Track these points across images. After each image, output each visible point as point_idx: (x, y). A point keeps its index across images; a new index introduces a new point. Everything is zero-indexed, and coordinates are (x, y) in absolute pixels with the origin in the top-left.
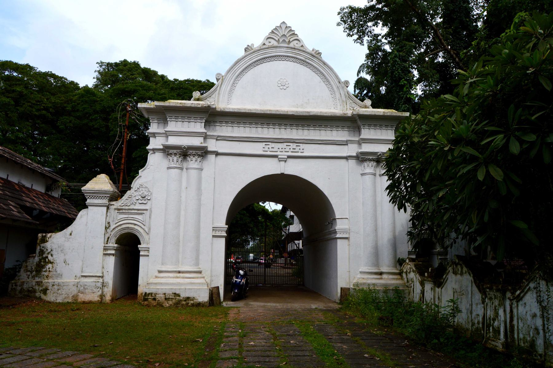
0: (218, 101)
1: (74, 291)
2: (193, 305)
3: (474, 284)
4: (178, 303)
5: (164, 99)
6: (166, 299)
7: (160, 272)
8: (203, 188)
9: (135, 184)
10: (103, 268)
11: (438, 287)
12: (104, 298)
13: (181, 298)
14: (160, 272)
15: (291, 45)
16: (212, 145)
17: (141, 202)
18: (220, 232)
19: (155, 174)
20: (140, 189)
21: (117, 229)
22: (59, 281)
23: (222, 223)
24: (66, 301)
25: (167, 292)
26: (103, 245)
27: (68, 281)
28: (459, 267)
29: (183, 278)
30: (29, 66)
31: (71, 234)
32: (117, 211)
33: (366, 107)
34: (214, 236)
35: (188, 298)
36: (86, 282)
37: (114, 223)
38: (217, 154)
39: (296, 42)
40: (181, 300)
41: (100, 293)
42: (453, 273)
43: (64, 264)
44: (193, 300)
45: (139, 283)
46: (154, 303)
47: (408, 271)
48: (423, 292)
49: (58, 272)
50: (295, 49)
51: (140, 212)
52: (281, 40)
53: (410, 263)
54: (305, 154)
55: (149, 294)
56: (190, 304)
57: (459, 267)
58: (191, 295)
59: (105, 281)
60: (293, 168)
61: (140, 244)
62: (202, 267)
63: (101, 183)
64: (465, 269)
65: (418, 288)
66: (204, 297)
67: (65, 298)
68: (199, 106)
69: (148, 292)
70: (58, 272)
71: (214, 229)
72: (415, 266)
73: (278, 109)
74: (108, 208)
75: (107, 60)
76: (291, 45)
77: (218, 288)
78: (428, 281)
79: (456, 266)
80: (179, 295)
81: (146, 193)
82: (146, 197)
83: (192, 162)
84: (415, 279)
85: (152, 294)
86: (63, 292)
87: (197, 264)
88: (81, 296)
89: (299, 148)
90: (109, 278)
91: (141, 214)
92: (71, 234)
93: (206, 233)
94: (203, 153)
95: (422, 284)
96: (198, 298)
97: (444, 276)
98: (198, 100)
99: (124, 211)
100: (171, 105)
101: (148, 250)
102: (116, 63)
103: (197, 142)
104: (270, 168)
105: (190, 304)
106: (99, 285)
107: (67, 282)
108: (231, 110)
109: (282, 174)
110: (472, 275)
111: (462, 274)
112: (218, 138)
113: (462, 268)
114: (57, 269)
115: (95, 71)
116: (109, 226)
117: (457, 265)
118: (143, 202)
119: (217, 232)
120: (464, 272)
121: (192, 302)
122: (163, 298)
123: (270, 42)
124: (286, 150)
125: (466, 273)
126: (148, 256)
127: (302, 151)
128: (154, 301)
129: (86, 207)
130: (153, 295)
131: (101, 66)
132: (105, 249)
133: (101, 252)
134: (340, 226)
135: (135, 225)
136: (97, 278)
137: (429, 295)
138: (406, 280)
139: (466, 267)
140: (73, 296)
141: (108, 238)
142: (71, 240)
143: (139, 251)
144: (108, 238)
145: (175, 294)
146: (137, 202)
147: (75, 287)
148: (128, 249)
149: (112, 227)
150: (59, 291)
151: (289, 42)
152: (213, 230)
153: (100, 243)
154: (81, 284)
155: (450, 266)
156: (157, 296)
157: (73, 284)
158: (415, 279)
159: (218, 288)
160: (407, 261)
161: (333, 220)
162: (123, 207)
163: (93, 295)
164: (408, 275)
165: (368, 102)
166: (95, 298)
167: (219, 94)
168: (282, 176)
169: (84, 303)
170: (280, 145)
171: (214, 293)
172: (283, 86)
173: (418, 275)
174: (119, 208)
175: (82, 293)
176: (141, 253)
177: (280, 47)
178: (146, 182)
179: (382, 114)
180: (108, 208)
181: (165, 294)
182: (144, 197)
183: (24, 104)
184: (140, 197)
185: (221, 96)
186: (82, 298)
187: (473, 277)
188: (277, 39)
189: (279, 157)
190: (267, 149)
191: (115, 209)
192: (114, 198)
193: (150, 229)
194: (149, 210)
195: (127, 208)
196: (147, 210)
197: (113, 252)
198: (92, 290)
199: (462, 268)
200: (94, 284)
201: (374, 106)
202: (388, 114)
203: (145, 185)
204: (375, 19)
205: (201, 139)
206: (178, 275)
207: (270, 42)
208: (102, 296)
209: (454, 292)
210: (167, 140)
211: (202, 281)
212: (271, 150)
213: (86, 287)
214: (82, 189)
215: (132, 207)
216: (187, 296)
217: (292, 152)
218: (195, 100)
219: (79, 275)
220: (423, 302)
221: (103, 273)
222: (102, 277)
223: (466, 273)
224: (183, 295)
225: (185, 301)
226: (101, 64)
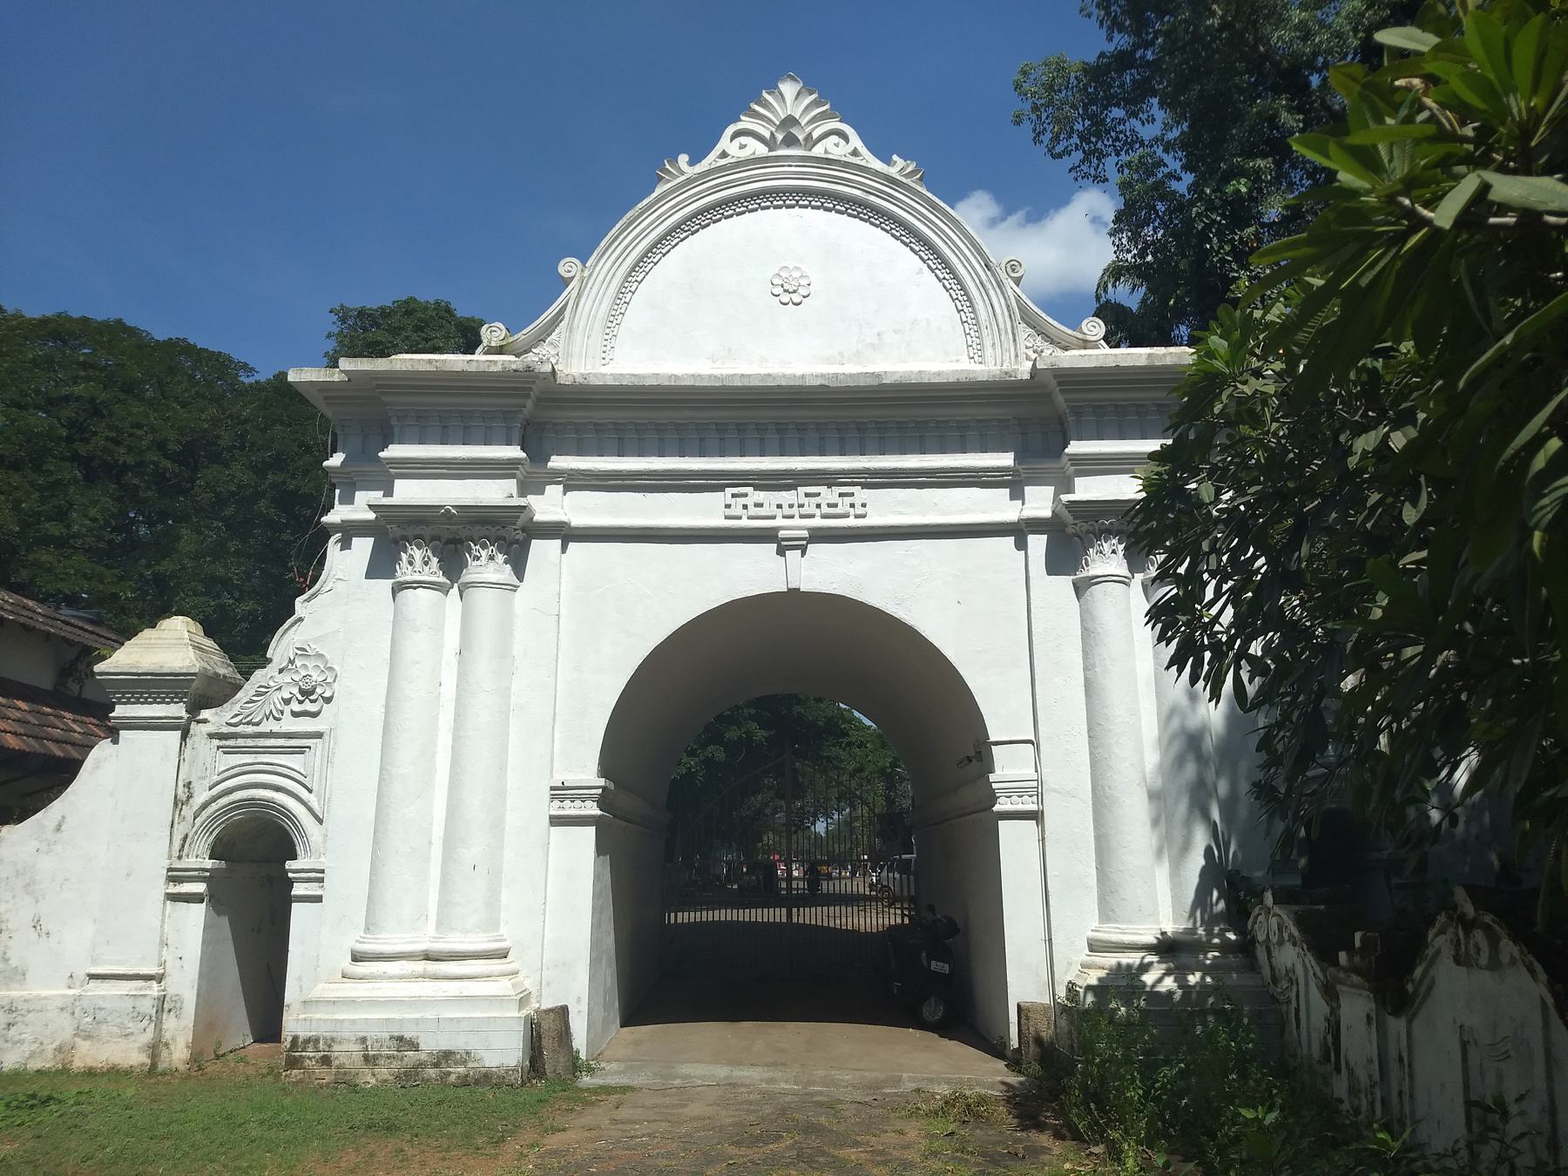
0: (569, 355)
1: (63, 1028)
2: (464, 1082)
3: (1555, 1020)
4: (410, 1077)
5: (384, 354)
6: (366, 1058)
7: (357, 958)
8: (517, 650)
9: (282, 647)
10: (164, 943)
11: (1396, 1012)
12: (165, 1053)
13: (423, 1057)
14: (357, 958)
15: (818, 151)
16: (550, 505)
17: (296, 707)
18: (578, 803)
19: (345, 612)
20: (298, 663)
21: (214, 806)
22: (14, 994)
23: (586, 771)
24: (35, 1065)
25: (373, 1033)
26: (166, 863)
27: (44, 993)
28: (1479, 936)
29: (436, 978)
30: (123, 325)
31: (58, 829)
32: (216, 742)
33: (1086, 344)
34: (557, 821)
35: (447, 1055)
36: (103, 997)
37: (207, 783)
38: (566, 534)
39: (834, 139)
40: (422, 1064)
41: (149, 1036)
42: (1457, 960)
43: (33, 935)
44: (464, 1062)
45: (286, 1001)
46: (326, 1075)
47: (1274, 939)
48: (1334, 1027)
49: (13, 963)
50: (829, 161)
51: (297, 744)
52: (780, 137)
53: (1277, 909)
54: (874, 519)
55: (307, 1041)
56: (453, 1078)
57: (1479, 936)
58: (456, 1043)
59: (171, 991)
60: (828, 572)
61: (293, 856)
62: (507, 934)
63: (172, 645)
64: (1508, 947)
65: (1318, 1007)
66: (503, 1051)
67: (32, 1055)
68: (493, 369)
69: (303, 1035)
70: (13, 963)
71: (560, 792)
72: (1300, 921)
73: (788, 371)
74: (185, 735)
75: (355, 302)
76: (818, 151)
77: (563, 1012)
78: (1352, 986)
79: (1467, 933)
80: (414, 1046)
81: (316, 677)
82: (319, 691)
83: (492, 564)
84: (1299, 970)
85: (317, 1040)
86: (26, 1032)
87: (492, 924)
88: (84, 1046)
89: (848, 500)
90: (184, 984)
91: (300, 750)
92: (58, 829)
93: (529, 806)
94: (511, 535)
95: (1330, 993)
96: (482, 1053)
97: (1418, 972)
98: (500, 350)
99: (241, 742)
100: (398, 368)
101: (318, 876)
102: (383, 309)
103: (494, 493)
104: (752, 573)
105: (453, 1078)
106: (147, 1007)
107: (39, 998)
108: (610, 382)
109: (794, 593)
110: (1543, 976)
111: (1495, 965)
112: (575, 482)
113: (1494, 943)
114: (9, 954)
115: (329, 336)
116: (190, 797)
117: (1468, 926)
118: (308, 706)
119: (567, 802)
120: (1505, 959)
121: (461, 1070)
122: (357, 1057)
123: (742, 147)
124: (803, 511)
125: (1513, 962)
126: (318, 899)
127: (860, 511)
128: (325, 1069)
129: (113, 733)
130: (321, 1046)
131: (343, 321)
132: (174, 877)
133: (161, 888)
134: (1008, 767)
135: (278, 789)
136: (140, 983)
137: (1358, 1042)
138: (1266, 971)
139: (1516, 938)
140: (59, 1049)
141: (186, 837)
142: (59, 848)
143: (290, 884)
144: (186, 837)
145: (400, 1039)
146: (287, 710)
147: (67, 1015)
148: (252, 873)
149: (201, 796)
150: (13, 1030)
151: (810, 142)
152: (553, 797)
153: (155, 857)
154: (85, 1003)
155: (1442, 932)
156: (336, 1047)
157: (60, 1005)
158: (1299, 970)
159: (563, 1012)
160: (1269, 898)
161: (979, 753)
162: (240, 729)
163: (123, 1043)
164: (1275, 953)
165: (1095, 328)
166: (131, 1055)
167: (570, 329)
168: (793, 596)
169: (90, 1073)
170: (786, 497)
171: (545, 1033)
172: (790, 293)
173: (1310, 959)
174: (226, 730)
175: (88, 1037)
176: (298, 890)
177: (778, 158)
178: (316, 640)
179: (1142, 362)
180: (185, 735)
181: (364, 1040)
182: (312, 692)
183: (95, 433)
184: (295, 691)
185: (578, 336)
186: (89, 1055)
187: (1551, 985)
188: (767, 135)
189: (782, 534)
190: (738, 511)
191: (211, 736)
192: (204, 694)
193: (325, 801)
194: (326, 737)
195: (250, 729)
196: (319, 735)
197: (200, 888)
198: (121, 1026)
199: (1494, 943)
200: (130, 1003)
201: (1111, 340)
202: (1168, 361)
203: (316, 647)
204: (1134, 101)
205: (510, 485)
206: (433, 967)
207: (742, 147)
208: (155, 1049)
209: (1464, 1046)
210: (389, 492)
211: (503, 987)
212: (753, 511)
213: (100, 1015)
214: (97, 668)
215: (266, 727)
216: (445, 1046)
217: (824, 516)
218: (491, 351)
219: (81, 973)
220: (1338, 1069)
221: (162, 964)
222: (159, 978)
223: (1513, 962)
224: (431, 1044)
225: (436, 1065)
226: (343, 315)
